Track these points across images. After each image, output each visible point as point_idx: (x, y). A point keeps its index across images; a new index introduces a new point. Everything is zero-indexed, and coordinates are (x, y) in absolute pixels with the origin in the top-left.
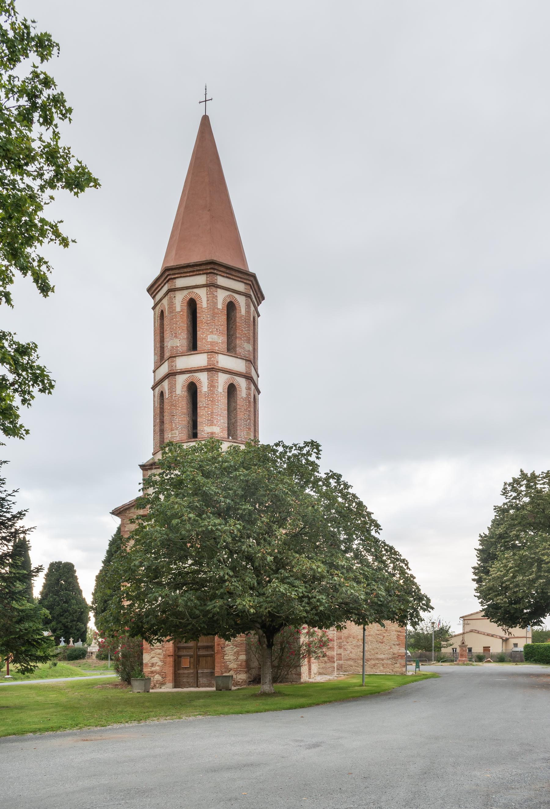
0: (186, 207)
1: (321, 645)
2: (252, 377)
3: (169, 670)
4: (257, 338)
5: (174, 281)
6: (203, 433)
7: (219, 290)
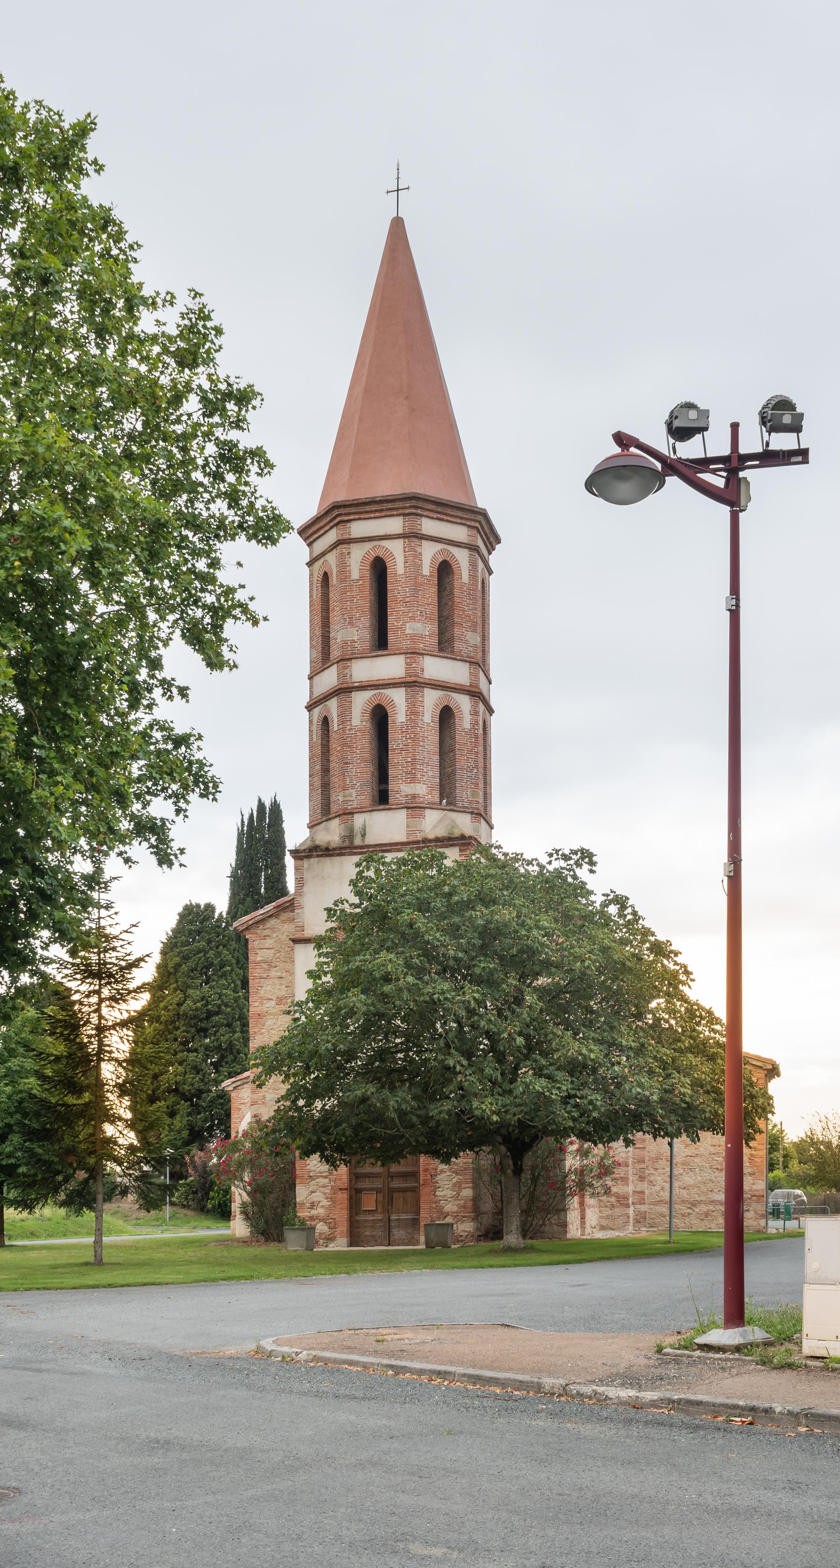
0: (367, 390)
1: (600, 1173)
2: (481, 693)
3: (342, 1215)
4: (489, 615)
5: (348, 525)
6: (398, 796)
7: (424, 542)
